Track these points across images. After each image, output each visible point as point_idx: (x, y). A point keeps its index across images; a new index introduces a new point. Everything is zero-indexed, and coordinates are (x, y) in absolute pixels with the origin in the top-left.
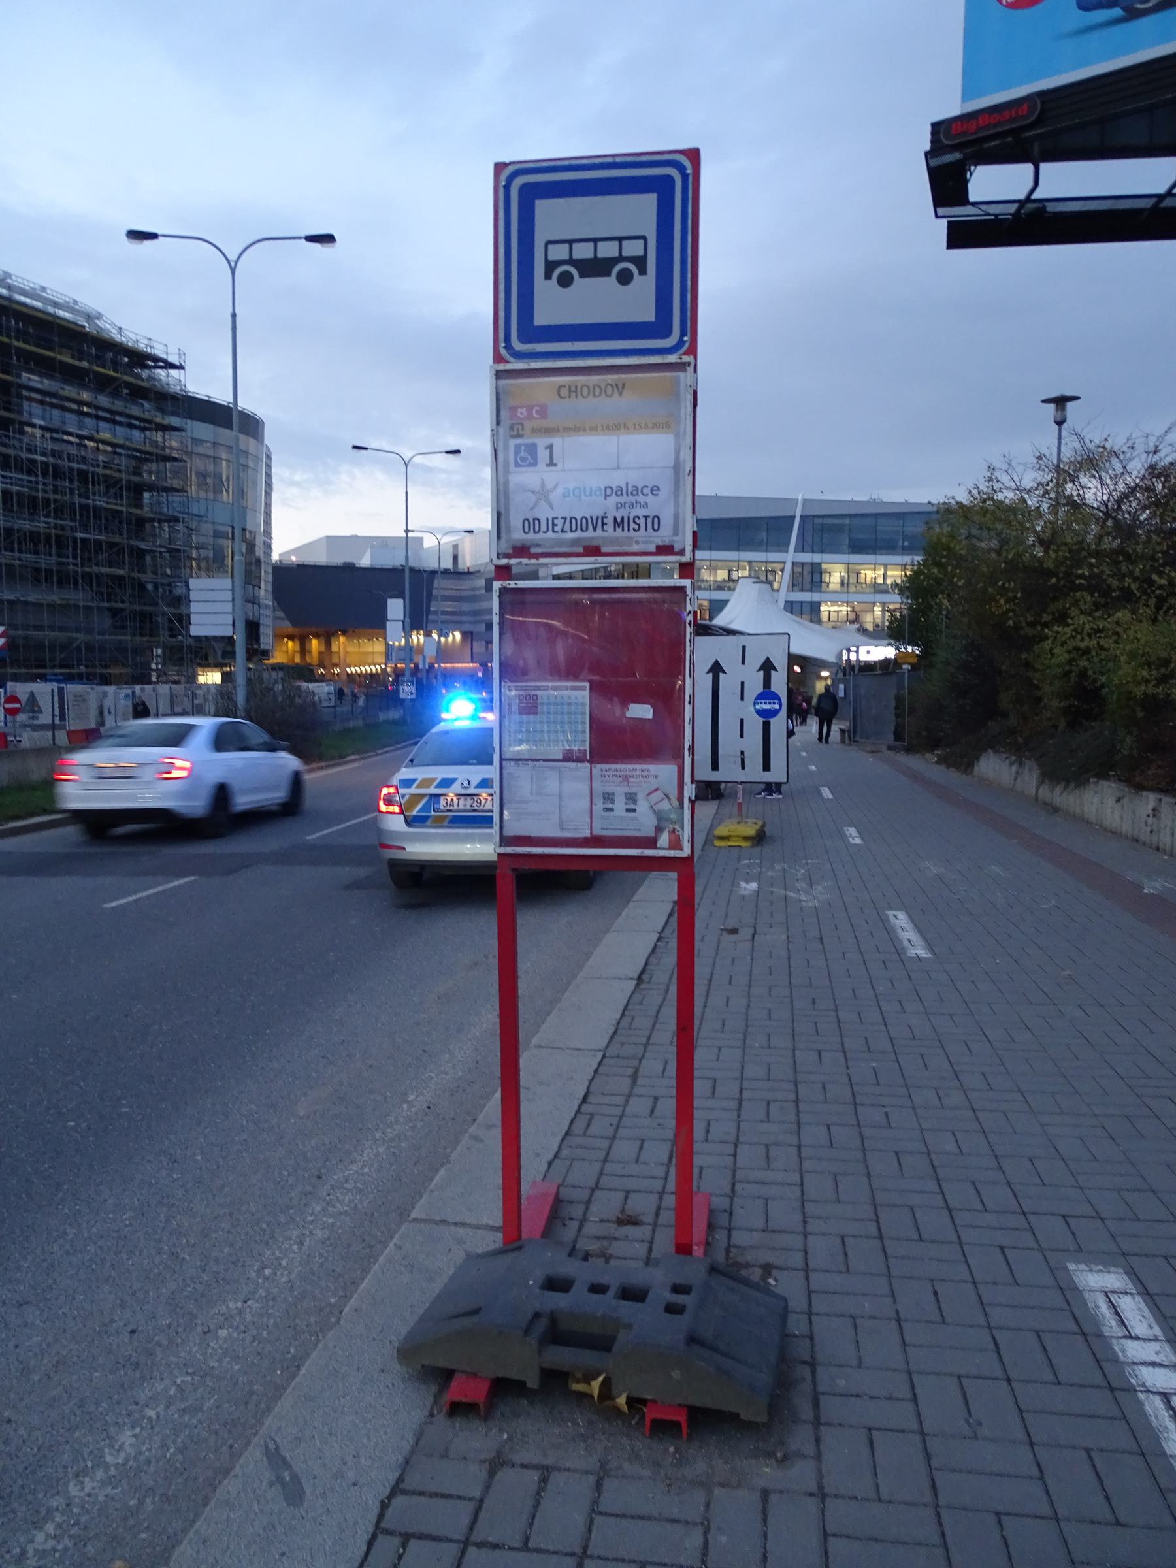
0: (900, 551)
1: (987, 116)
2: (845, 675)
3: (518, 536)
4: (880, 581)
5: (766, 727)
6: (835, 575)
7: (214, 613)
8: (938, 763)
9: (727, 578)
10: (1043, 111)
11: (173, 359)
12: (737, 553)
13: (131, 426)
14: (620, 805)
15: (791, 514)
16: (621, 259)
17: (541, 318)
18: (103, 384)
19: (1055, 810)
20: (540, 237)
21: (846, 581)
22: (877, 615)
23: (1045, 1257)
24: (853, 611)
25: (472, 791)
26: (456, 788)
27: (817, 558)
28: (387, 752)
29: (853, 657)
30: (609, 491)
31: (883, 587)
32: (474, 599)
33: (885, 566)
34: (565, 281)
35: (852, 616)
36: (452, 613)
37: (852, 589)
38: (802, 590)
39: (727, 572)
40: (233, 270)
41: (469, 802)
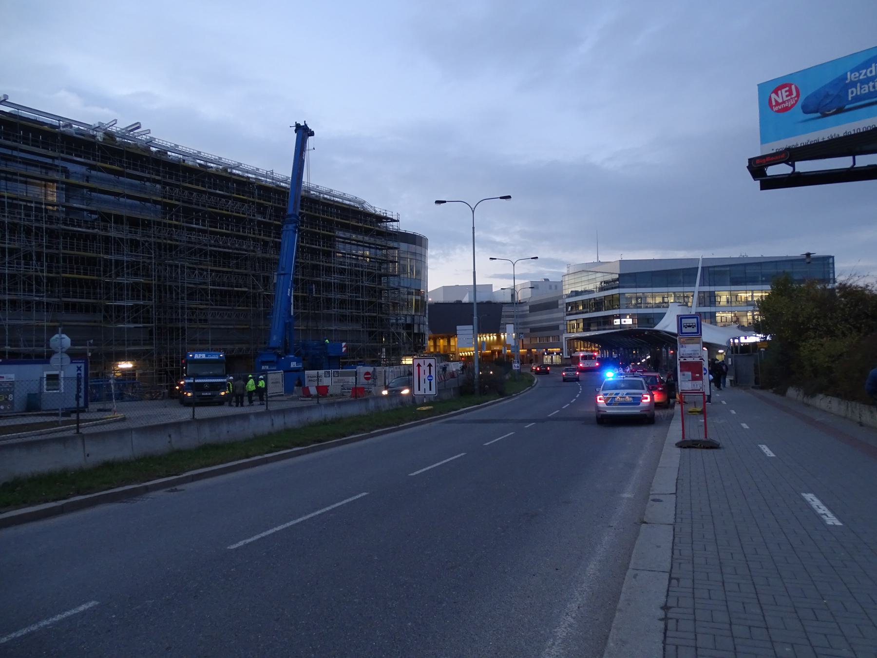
2: (732, 353)
3: (682, 355)
4: (750, 299)
5: (430, 383)
6: (723, 297)
8: (773, 393)
9: (662, 301)
11: (395, 218)
12: (667, 288)
13: (377, 248)
14: (695, 386)
15: (697, 266)
17: (683, 332)
18: (367, 232)
19: (809, 405)
20: (683, 323)
21: (730, 300)
22: (748, 318)
24: (735, 316)
25: (624, 396)
26: (620, 395)
27: (712, 289)
29: (736, 341)
30: (692, 351)
31: (752, 303)
34: (686, 328)
35: (734, 319)
37: (734, 304)
38: (705, 306)
39: (661, 298)
40: (473, 212)
41: (623, 399)
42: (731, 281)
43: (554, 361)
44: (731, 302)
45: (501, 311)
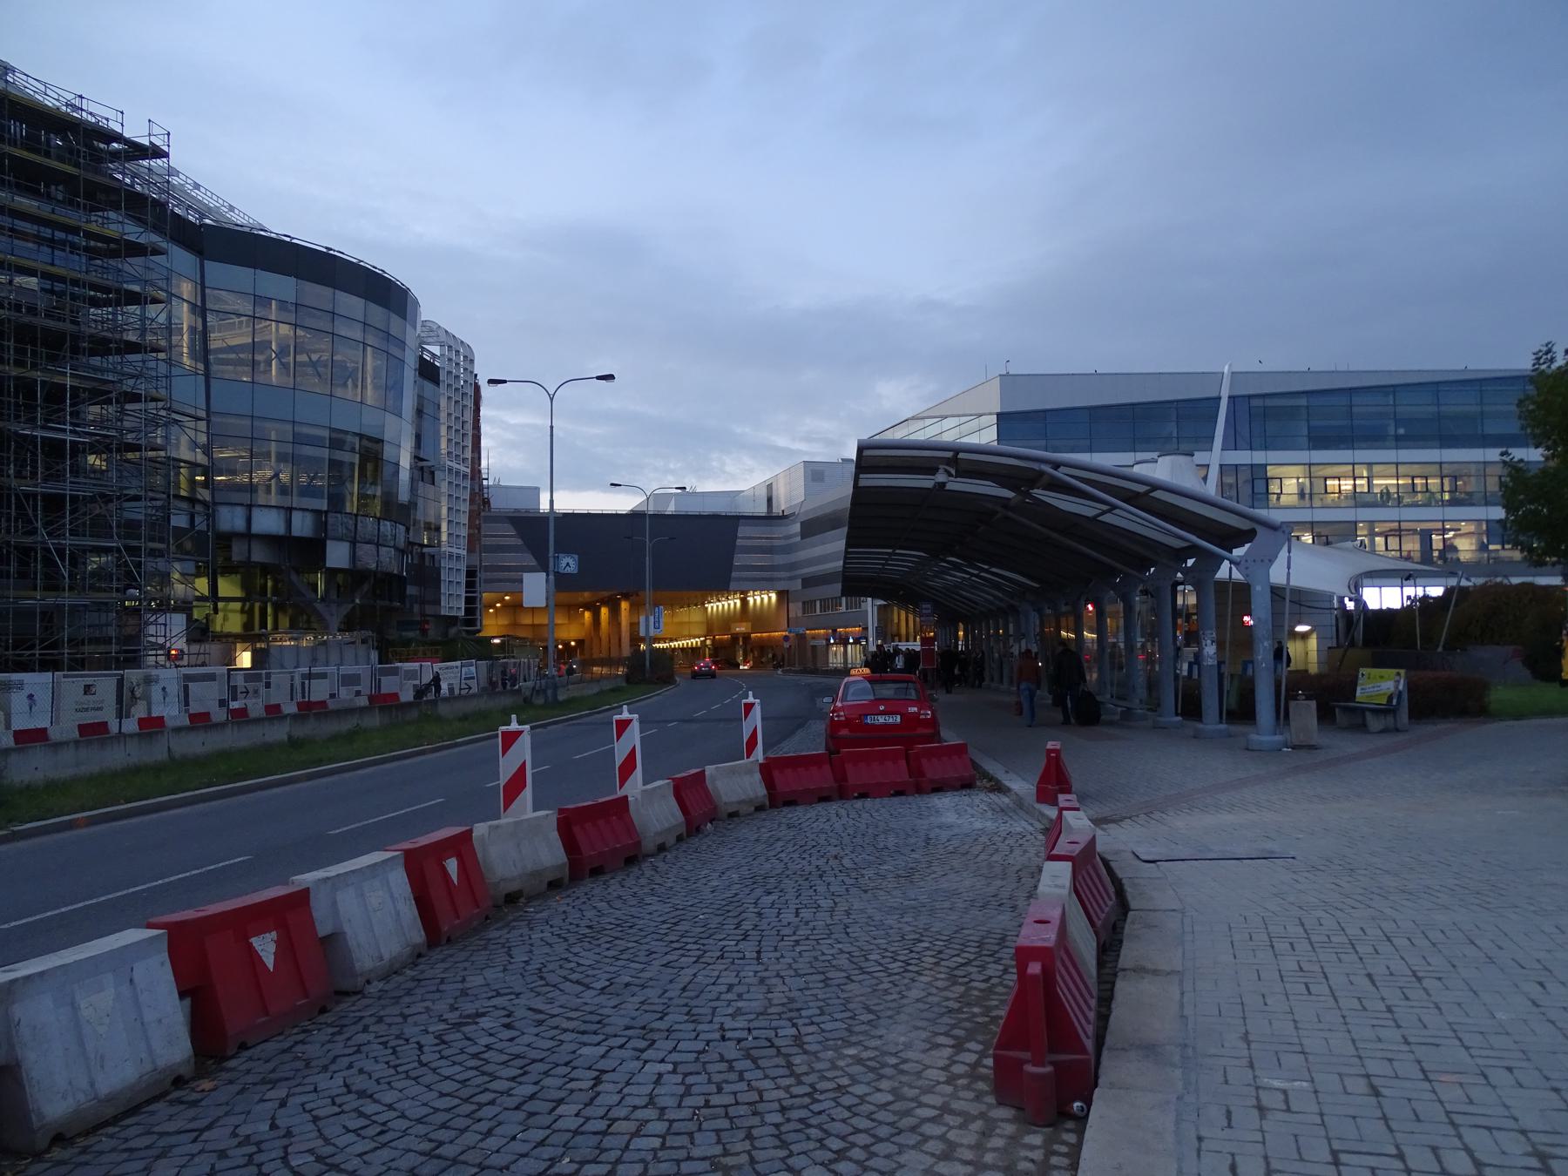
0: (1394, 443)
12: (1350, 452)
15: (1215, 394)
21: (1307, 491)
27: (1258, 457)
31: (1369, 498)
32: (788, 549)
33: (1370, 465)
36: (761, 568)
37: (1317, 503)
40: (552, 400)
42: (1310, 438)
43: (849, 661)
44: (1311, 494)
45: (736, 537)
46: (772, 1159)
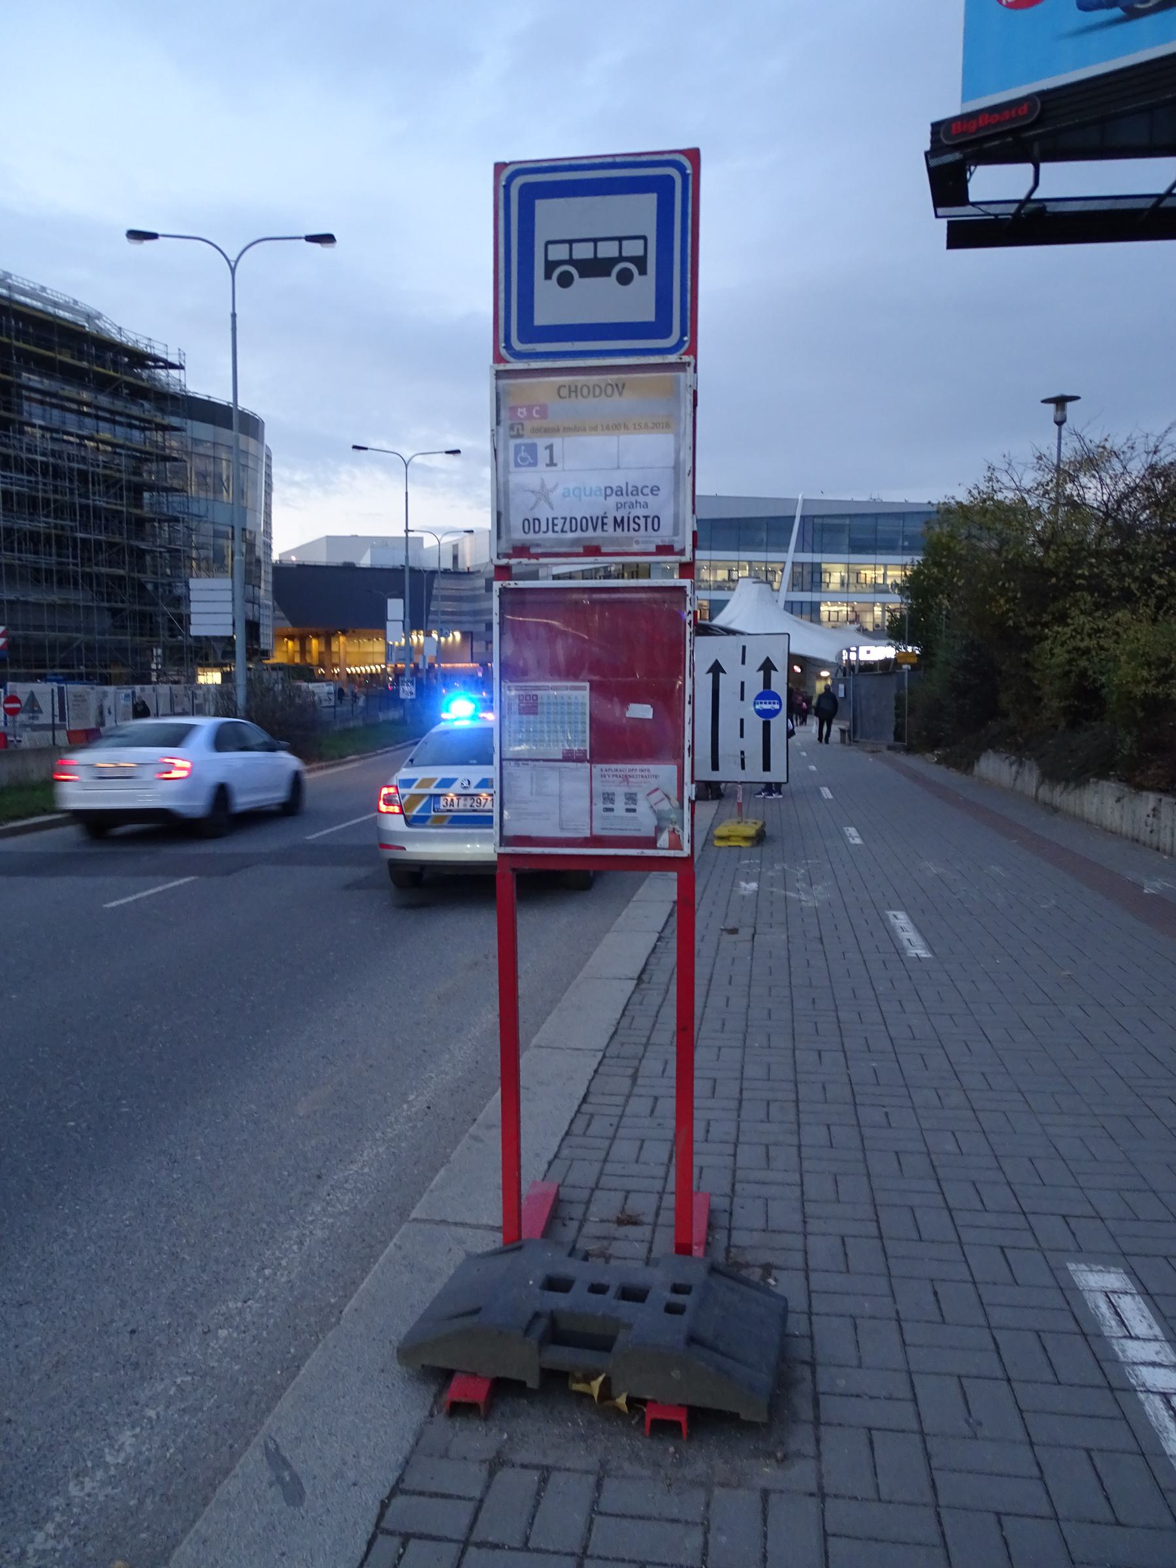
0: (900, 551)
1: (987, 116)
2: (845, 675)
3: (518, 536)
4: (880, 581)
6: (835, 575)
7: (214, 613)
8: (938, 763)
9: (727, 578)
10: (1043, 111)
11: (173, 359)
12: (737, 553)
13: (131, 426)
14: (620, 805)
15: (791, 514)
16: (621, 259)
17: (541, 318)
18: (103, 384)
19: (1055, 810)
20: (540, 237)
21: (846, 581)
22: (877, 615)
23: (1045, 1257)
24: (853, 611)
25: (472, 791)
26: (456, 788)
27: (817, 558)
28: (387, 752)
29: (853, 657)
30: (609, 491)
31: (883, 587)
32: (474, 599)
33: (885, 566)
34: (565, 281)
35: (852, 616)
36: (452, 613)
37: (852, 589)
38: (802, 590)
39: (727, 572)
40: (233, 270)
41: (469, 802)
46: (584, 1160)
